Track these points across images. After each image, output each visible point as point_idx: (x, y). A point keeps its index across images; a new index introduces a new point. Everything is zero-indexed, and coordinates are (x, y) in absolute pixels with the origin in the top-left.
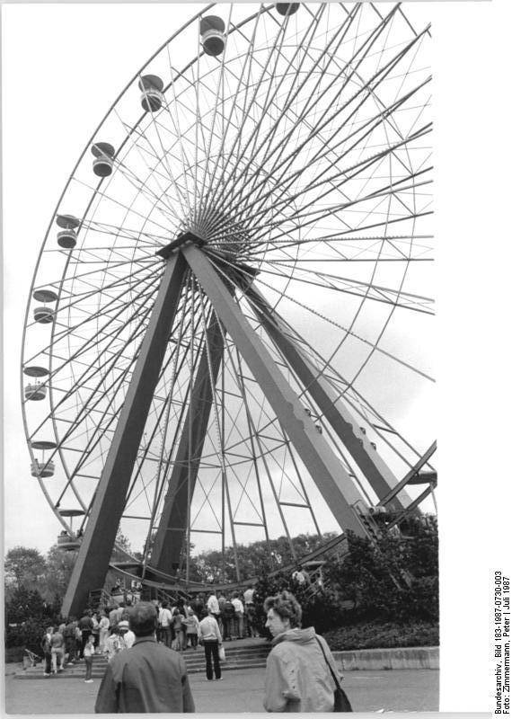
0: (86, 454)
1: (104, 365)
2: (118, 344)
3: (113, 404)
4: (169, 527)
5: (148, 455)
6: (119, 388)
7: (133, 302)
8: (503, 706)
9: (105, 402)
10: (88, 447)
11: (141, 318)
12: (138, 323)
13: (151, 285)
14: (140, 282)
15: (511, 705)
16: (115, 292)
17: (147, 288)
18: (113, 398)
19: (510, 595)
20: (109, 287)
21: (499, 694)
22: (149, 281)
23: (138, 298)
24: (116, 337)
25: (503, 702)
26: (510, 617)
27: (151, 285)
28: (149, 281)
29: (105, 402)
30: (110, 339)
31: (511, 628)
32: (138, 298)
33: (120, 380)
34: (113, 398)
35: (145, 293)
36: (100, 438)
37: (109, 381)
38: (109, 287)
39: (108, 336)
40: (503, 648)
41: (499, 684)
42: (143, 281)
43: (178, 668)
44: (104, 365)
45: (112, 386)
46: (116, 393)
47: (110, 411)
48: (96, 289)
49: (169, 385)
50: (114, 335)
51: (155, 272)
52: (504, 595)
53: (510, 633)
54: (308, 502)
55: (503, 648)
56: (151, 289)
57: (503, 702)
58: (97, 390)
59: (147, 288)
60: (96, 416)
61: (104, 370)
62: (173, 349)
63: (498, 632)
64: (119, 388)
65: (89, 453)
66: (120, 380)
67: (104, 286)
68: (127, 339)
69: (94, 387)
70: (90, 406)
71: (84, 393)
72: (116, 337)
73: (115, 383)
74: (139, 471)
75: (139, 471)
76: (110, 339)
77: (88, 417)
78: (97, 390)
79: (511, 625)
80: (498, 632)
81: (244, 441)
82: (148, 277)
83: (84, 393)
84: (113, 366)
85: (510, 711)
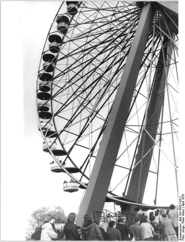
0: (64, 106)
1: (85, 62)
2: (96, 42)
3: (85, 83)
4: (44, 81)
5: (98, 115)
6: (90, 76)
7: (111, 22)
8: (182, 238)
9: (81, 82)
10: (66, 102)
11: (112, 33)
12: (110, 35)
13: (125, 16)
14: (120, 12)
15: (184, 237)
16: (105, 13)
17: (122, 17)
18: (86, 80)
19: (184, 200)
20: (103, 9)
21: (181, 234)
22: (125, 14)
23: (115, 21)
24: (96, 38)
25: (182, 236)
26: (184, 209)
27: (125, 16)
28: (125, 14)
29: (81, 82)
30: (93, 37)
31: (184, 220)
32: (115, 21)
33: (89, 61)
34: (86, 80)
35: (119, 20)
36: (74, 99)
37: (86, 71)
38: (103, 9)
39: (93, 35)
40: (182, 218)
41: (181, 230)
42: (121, 12)
43: (134, 229)
44: (85, 62)
45: (88, 74)
46: (88, 78)
47: (82, 87)
48: (97, 8)
49: (112, 75)
50: (96, 36)
51: (130, 10)
52: (182, 200)
53: (184, 222)
54: (158, 172)
55: (182, 218)
56: (124, 19)
57: (182, 236)
58: (77, 74)
59: (122, 17)
60: (75, 87)
61: (84, 65)
62: (122, 56)
63: (180, 213)
64: (90, 76)
65: (66, 106)
66: (89, 61)
67: (102, 8)
68: (102, 40)
69: (77, 72)
70: (73, 81)
71: (71, 74)
72: (96, 38)
73: (89, 73)
74: (80, 112)
75: (80, 112)
76: (93, 37)
77: (70, 87)
78: (77, 74)
79: (184, 219)
80: (180, 213)
81: (139, 126)
82: (125, 12)
83: (71, 74)
84: (88, 53)
85: (184, 239)
